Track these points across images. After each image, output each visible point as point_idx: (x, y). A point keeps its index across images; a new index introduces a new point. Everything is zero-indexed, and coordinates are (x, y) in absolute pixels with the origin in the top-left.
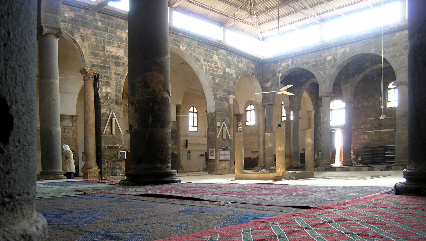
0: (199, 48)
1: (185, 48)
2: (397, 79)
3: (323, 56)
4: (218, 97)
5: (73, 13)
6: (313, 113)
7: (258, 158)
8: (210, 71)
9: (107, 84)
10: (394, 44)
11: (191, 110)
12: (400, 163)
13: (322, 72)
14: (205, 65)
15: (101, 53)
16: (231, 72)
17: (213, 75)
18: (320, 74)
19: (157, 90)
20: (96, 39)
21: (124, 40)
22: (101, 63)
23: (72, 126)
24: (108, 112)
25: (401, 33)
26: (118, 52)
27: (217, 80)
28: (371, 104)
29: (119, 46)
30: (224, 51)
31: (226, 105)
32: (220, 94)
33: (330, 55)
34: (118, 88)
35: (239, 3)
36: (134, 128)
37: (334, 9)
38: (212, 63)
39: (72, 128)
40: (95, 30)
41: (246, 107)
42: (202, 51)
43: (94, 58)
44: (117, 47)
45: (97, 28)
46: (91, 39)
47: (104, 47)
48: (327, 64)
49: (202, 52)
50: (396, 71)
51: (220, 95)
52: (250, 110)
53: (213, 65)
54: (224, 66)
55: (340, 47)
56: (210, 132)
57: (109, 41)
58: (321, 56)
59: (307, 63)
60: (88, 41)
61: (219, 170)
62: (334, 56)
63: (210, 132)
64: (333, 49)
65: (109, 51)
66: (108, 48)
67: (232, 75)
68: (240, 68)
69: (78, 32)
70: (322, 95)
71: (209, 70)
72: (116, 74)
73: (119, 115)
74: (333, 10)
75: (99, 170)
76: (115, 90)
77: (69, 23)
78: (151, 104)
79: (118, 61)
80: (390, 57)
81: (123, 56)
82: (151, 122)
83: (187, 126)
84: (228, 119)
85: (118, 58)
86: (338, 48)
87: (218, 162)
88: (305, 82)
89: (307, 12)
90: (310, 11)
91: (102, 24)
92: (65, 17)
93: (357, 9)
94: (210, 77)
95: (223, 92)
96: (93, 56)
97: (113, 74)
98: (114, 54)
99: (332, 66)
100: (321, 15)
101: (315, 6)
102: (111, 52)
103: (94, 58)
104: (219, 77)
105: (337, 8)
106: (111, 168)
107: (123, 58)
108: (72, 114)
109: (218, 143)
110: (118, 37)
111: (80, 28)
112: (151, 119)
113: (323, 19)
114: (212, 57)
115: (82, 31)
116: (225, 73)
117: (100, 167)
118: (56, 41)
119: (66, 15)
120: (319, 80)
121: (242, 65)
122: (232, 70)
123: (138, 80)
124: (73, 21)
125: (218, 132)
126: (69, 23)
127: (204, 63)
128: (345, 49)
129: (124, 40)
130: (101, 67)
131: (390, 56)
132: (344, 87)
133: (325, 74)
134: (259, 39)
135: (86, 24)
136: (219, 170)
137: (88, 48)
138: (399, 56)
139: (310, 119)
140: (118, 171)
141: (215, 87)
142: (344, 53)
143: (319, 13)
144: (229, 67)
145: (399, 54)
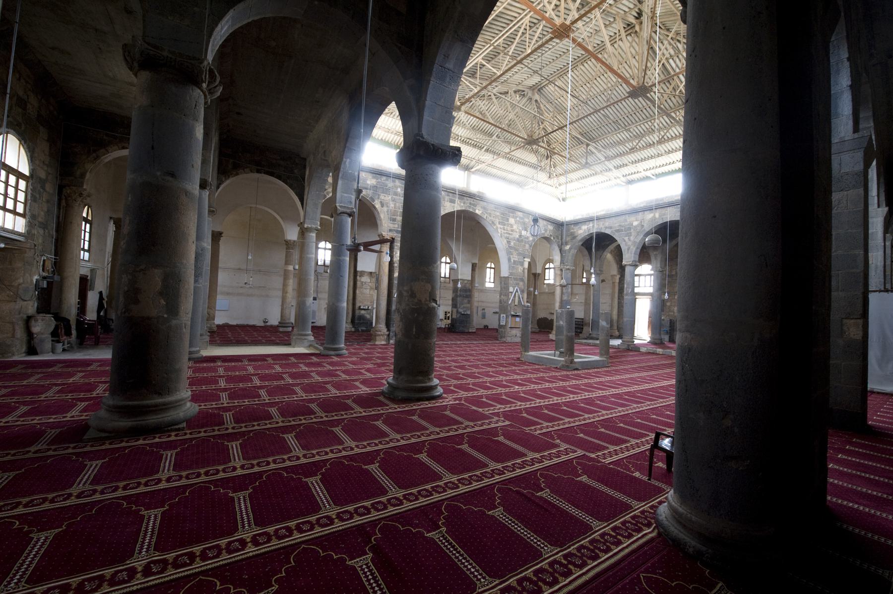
1: (481, 212)
3: (628, 220)
6: (618, 277)
11: (489, 265)
13: (626, 239)
17: (508, 239)
18: (625, 241)
19: (423, 300)
20: (395, 204)
27: (512, 244)
30: (521, 213)
31: (520, 269)
32: (515, 257)
33: (636, 220)
36: (398, 336)
39: (370, 284)
41: (545, 264)
42: (498, 214)
52: (549, 268)
53: (509, 228)
54: (521, 228)
55: (648, 212)
56: (502, 296)
58: (626, 220)
59: (611, 228)
60: (387, 207)
62: (641, 222)
63: (502, 296)
67: (528, 238)
69: (378, 198)
70: (626, 263)
71: (504, 233)
75: (387, 333)
78: (416, 315)
82: (414, 333)
83: (484, 281)
84: (521, 283)
87: (509, 330)
88: (608, 245)
90: (616, 173)
92: (368, 184)
93: (671, 170)
94: (505, 241)
99: (638, 232)
101: (620, 167)
104: (514, 240)
108: (370, 271)
109: (509, 308)
112: (414, 330)
114: (508, 220)
115: (382, 197)
116: (520, 236)
117: (389, 330)
118: (349, 220)
119: (369, 182)
120: (624, 248)
123: (405, 288)
124: (375, 188)
126: (370, 190)
127: (499, 226)
132: (652, 254)
133: (630, 240)
134: (559, 199)
137: (386, 213)
139: (614, 283)
141: (510, 250)
144: (526, 230)
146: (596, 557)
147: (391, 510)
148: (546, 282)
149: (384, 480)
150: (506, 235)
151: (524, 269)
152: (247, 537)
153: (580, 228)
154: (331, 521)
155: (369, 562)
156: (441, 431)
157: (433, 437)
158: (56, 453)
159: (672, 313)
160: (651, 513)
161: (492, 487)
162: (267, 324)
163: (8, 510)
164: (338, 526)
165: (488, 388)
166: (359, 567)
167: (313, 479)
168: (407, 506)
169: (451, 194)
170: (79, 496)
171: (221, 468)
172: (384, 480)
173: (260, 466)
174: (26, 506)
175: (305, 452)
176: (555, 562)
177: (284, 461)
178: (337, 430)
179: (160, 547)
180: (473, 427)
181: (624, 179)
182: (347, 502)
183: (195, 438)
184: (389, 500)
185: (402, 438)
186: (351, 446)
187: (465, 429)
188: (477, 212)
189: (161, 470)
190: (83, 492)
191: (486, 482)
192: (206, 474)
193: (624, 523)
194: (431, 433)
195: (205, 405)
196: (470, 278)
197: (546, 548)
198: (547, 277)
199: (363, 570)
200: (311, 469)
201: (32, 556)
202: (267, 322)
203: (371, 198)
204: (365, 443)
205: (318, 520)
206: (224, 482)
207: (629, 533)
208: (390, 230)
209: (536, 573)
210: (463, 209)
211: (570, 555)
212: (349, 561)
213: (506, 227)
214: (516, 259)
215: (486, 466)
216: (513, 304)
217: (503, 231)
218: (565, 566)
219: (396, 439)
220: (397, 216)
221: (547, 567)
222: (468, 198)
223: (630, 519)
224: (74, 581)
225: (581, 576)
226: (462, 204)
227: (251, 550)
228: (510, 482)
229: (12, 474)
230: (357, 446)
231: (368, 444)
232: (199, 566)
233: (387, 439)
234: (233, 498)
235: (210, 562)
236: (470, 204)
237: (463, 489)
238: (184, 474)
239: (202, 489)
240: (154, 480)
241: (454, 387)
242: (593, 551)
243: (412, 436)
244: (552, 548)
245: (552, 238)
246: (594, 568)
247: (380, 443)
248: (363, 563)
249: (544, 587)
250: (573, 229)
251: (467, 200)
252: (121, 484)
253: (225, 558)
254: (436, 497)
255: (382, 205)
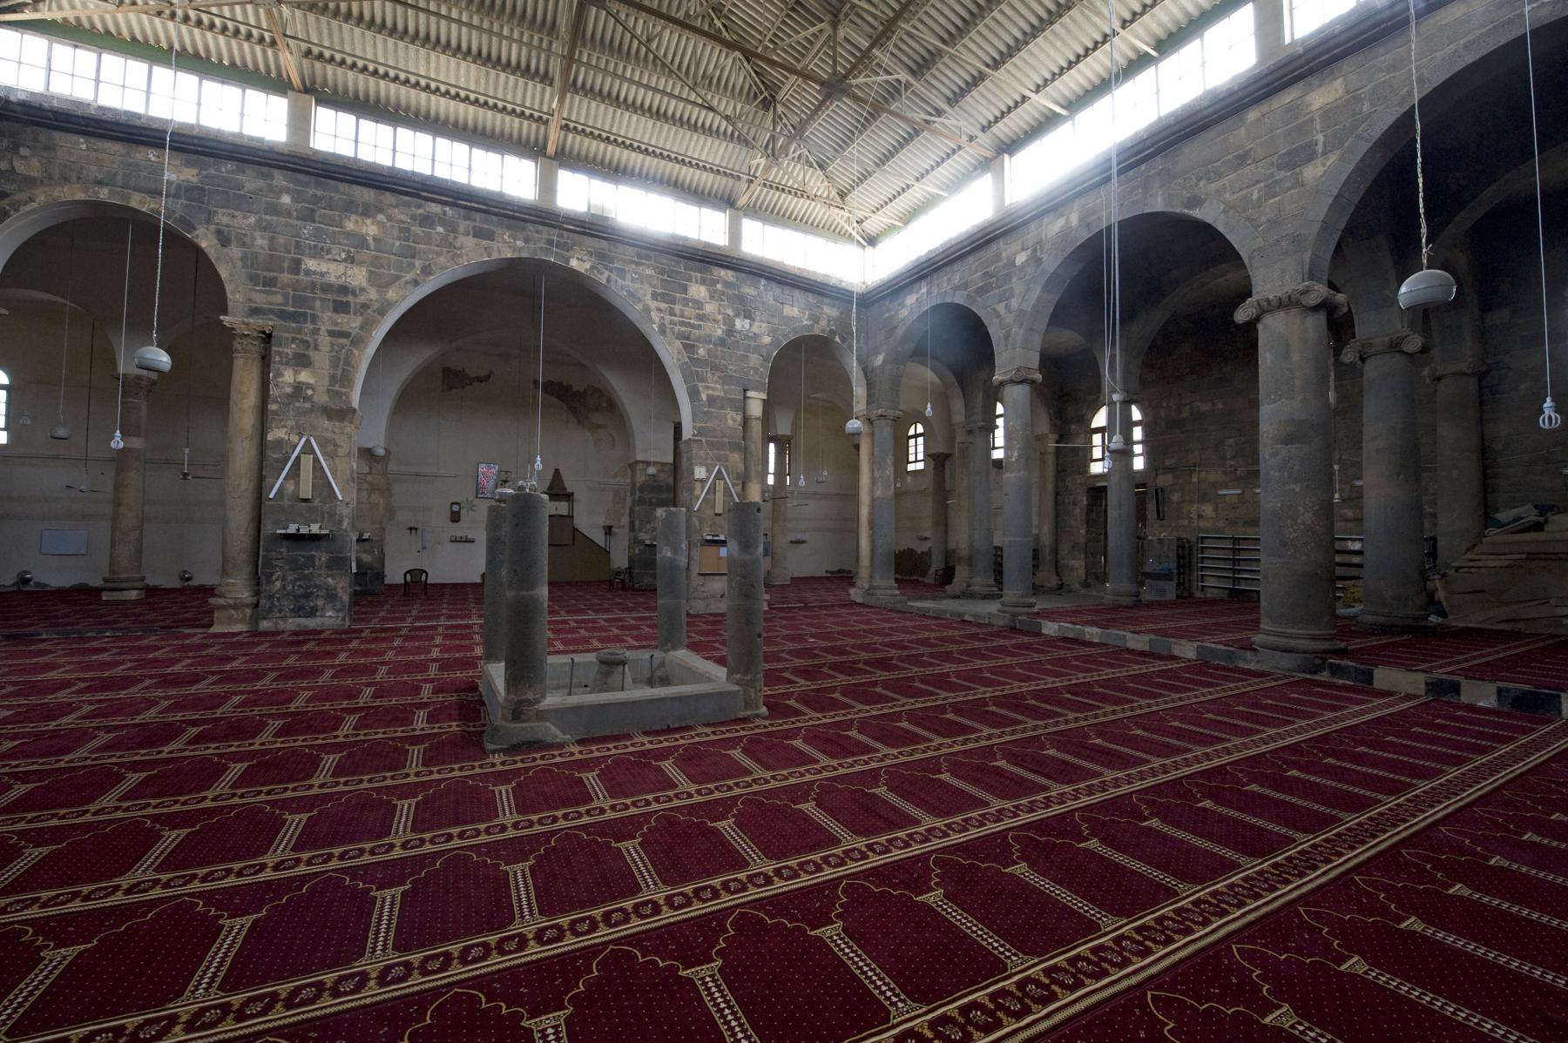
0: (637, 264)
1: (587, 265)
2: (1254, 291)
4: (704, 397)
5: (195, 171)
7: (929, 553)
8: (677, 328)
9: (302, 361)
10: (1239, 157)
12: (1285, 640)
13: (1001, 308)
14: (659, 310)
15: (286, 277)
16: (755, 329)
17: (688, 338)
18: (998, 315)
20: (272, 239)
21: (371, 242)
22: (286, 304)
23: (370, 473)
24: (294, 438)
25: (1265, 107)
26: (345, 274)
27: (701, 351)
28: (1220, 406)
29: (350, 260)
32: (712, 388)
33: (1023, 249)
34: (339, 373)
35: (660, 101)
37: (1028, 93)
38: (686, 305)
40: (268, 217)
42: (649, 272)
43: (261, 291)
44: (345, 260)
45: (275, 210)
46: (253, 238)
47: (298, 262)
48: (1014, 280)
49: (651, 276)
50: (1250, 259)
51: (711, 392)
52: (916, 436)
54: (730, 312)
55: (1052, 216)
57: (316, 246)
60: (244, 245)
61: (702, 599)
62: (1035, 250)
64: (1032, 226)
65: (315, 273)
66: (311, 264)
67: (756, 336)
68: (787, 317)
69: (208, 221)
71: (672, 323)
72: (332, 334)
73: (335, 445)
74: (1024, 99)
76: (327, 379)
77: (179, 198)
79: (344, 299)
80: (1225, 212)
81: (364, 284)
85: (344, 290)
86: (1046, 220)
89: (945, 121)
90: (953, 120)
91: (294, 200)
94: (678, 344)
95: (723, 384)
96: (257, 284)
97: (323, 332)
98: (332, 279)
100: (994, 129)
102: (322, 275)
103: (261, 291)
105: (1033, 88)
106: (296, 597)
107: (362, 290)
110: (349, 234)
111: (216, 212)
113: (1008, 142)
114: (685, 289)
115: (223, 217)
121: (795, 309)
122: (757, 324)
125: (697, 492)
127: (653, 304)
128: (1068, 221)
129: (371, 242)
130: (282, 315)
131: (1222, 206)
135: (240, 202)
136: (702, 599)
137: (239, 264)
138: (1259, 199)
140: (320, 602)
142: (1065, 234)
143: (985, 124)
144: (748, 315)
145: (1260, 191)
146: (1188, 931)
147: (753, 893)
148: (911, 467)
149: (741, 843)
150: (677, 328)
151: (746, 421)
152: (529, 931)
153: (902, 305)
154: (656, 909)
155: (559, 1025)
156: (900, 753)
157: (826, 774)
158: (244, 801)
159: (1186, 522)
160: (1178, 922)
161: (924, 858)
162: (190, 583)
163: (101, 898)
164: (668, 916)
165: (918, 693)
166: (539, 1031)
167: (628, 844)
168: (780, 886)
169: (478, 216)
170: (276, 868)
171: (482, 826)
172: (741, 843)
173: (543, 825)
174: (204, 879)
175: (697, 787)
176: (1028, 980)
177: (580, 815)
178: (667, 765)
179: (402, 945)
180: (896, 757)
181: (984, 139)
182: (685, 878)
183: (445, 780)
184: (750, 877)
185: (773, 777)
186: (687, 791)
187: (882, 760)
188: (574, 263)
189: (393, 830)
190: (283, 862)
191: (916, 849)
192: (461, 835)
193: (1159, 920)
194: (823, 768)
195: (384, 733)
196: (670, 459)
197: (1014, 958)
198: (912, 458)
199: (704, 984)
200: (623, 829)
201: (221, 954)
202: (189, 579)
203: (182, 220)
204: (711, 786)
205: (636, 907)
206: (493, 848)
207: (1167, 936)
208: (255, 311)
209: (993, 997)
210: (525, 255)
211: (1055, 968)
212: (528, 1019)
213: (677, 308)
214: (717, 393)
215: (917, 822)
216: (710, 512)
217: (668, 317)
218: (1046, 987)
219: (763, 779)
220: (282, 271)
221: (1013, 989)
222: (541, 228)
223: (1171, 914)
224: (131, 1022)
225: (1069, 1004)
226: (519, 243)
227: (534, 952)
228: (958, 850)
229: (184, 832)
230: (699, 792)
231: (717, 788)
232: (457, 972)
233: (748, 779)
234: (507, 873)
235: (197, 1035)
236: (550, 242)
237: (875, 860)
238: (427, 836)
239: (456, 861)
240: (384, 845)
241: (843, 694)
242: (1097, 964)
243: (790, 774)
244: (914, 1005)
245: (837, 339)
246: (1096, 991)
247: (737, 785)
248: (706, 975)
249: (976, 1035)
250: (888, 311)
251: (538, 232)
252: (337, 851)
253: (496, 962)
254: (828, 873)
255: (224, 239)
